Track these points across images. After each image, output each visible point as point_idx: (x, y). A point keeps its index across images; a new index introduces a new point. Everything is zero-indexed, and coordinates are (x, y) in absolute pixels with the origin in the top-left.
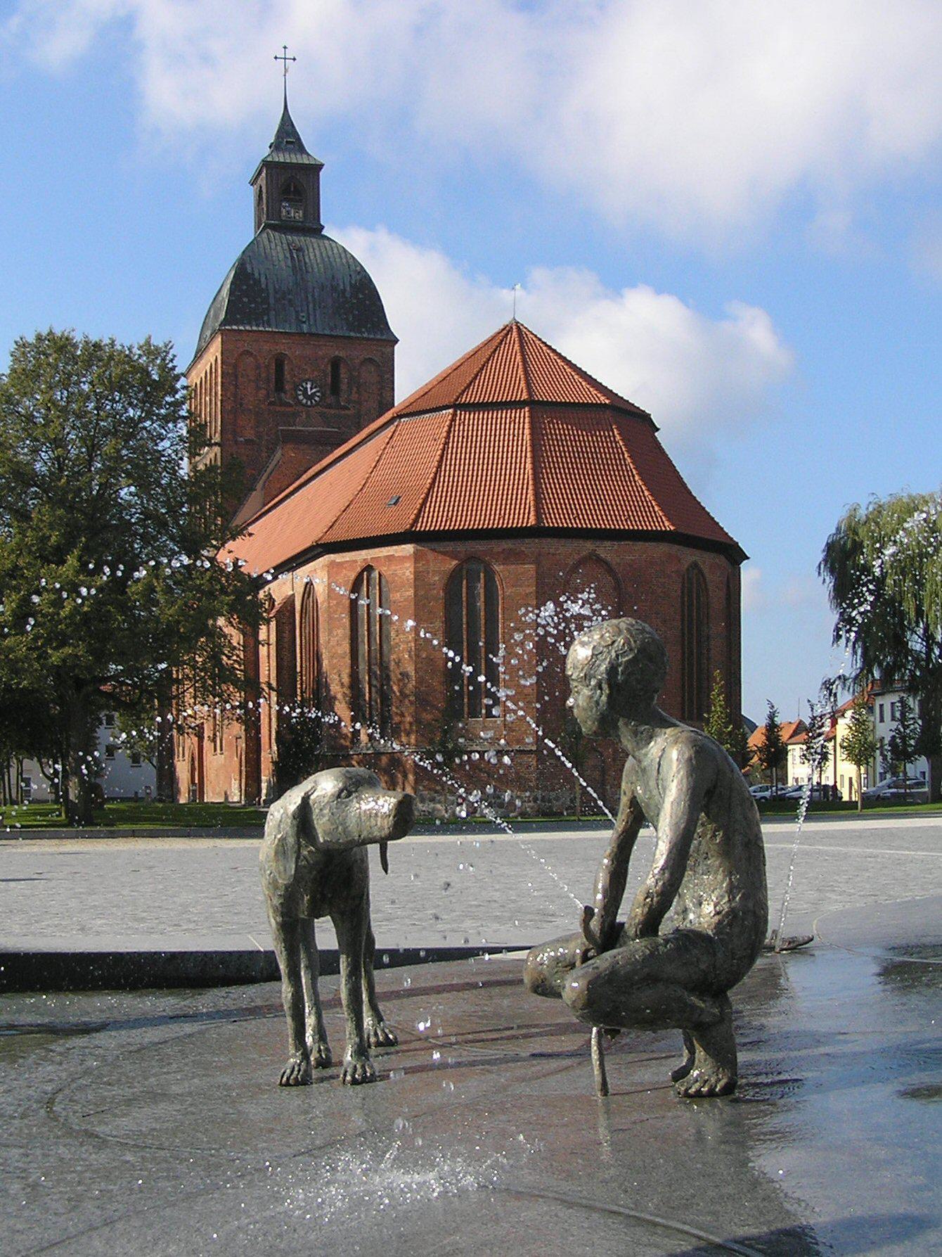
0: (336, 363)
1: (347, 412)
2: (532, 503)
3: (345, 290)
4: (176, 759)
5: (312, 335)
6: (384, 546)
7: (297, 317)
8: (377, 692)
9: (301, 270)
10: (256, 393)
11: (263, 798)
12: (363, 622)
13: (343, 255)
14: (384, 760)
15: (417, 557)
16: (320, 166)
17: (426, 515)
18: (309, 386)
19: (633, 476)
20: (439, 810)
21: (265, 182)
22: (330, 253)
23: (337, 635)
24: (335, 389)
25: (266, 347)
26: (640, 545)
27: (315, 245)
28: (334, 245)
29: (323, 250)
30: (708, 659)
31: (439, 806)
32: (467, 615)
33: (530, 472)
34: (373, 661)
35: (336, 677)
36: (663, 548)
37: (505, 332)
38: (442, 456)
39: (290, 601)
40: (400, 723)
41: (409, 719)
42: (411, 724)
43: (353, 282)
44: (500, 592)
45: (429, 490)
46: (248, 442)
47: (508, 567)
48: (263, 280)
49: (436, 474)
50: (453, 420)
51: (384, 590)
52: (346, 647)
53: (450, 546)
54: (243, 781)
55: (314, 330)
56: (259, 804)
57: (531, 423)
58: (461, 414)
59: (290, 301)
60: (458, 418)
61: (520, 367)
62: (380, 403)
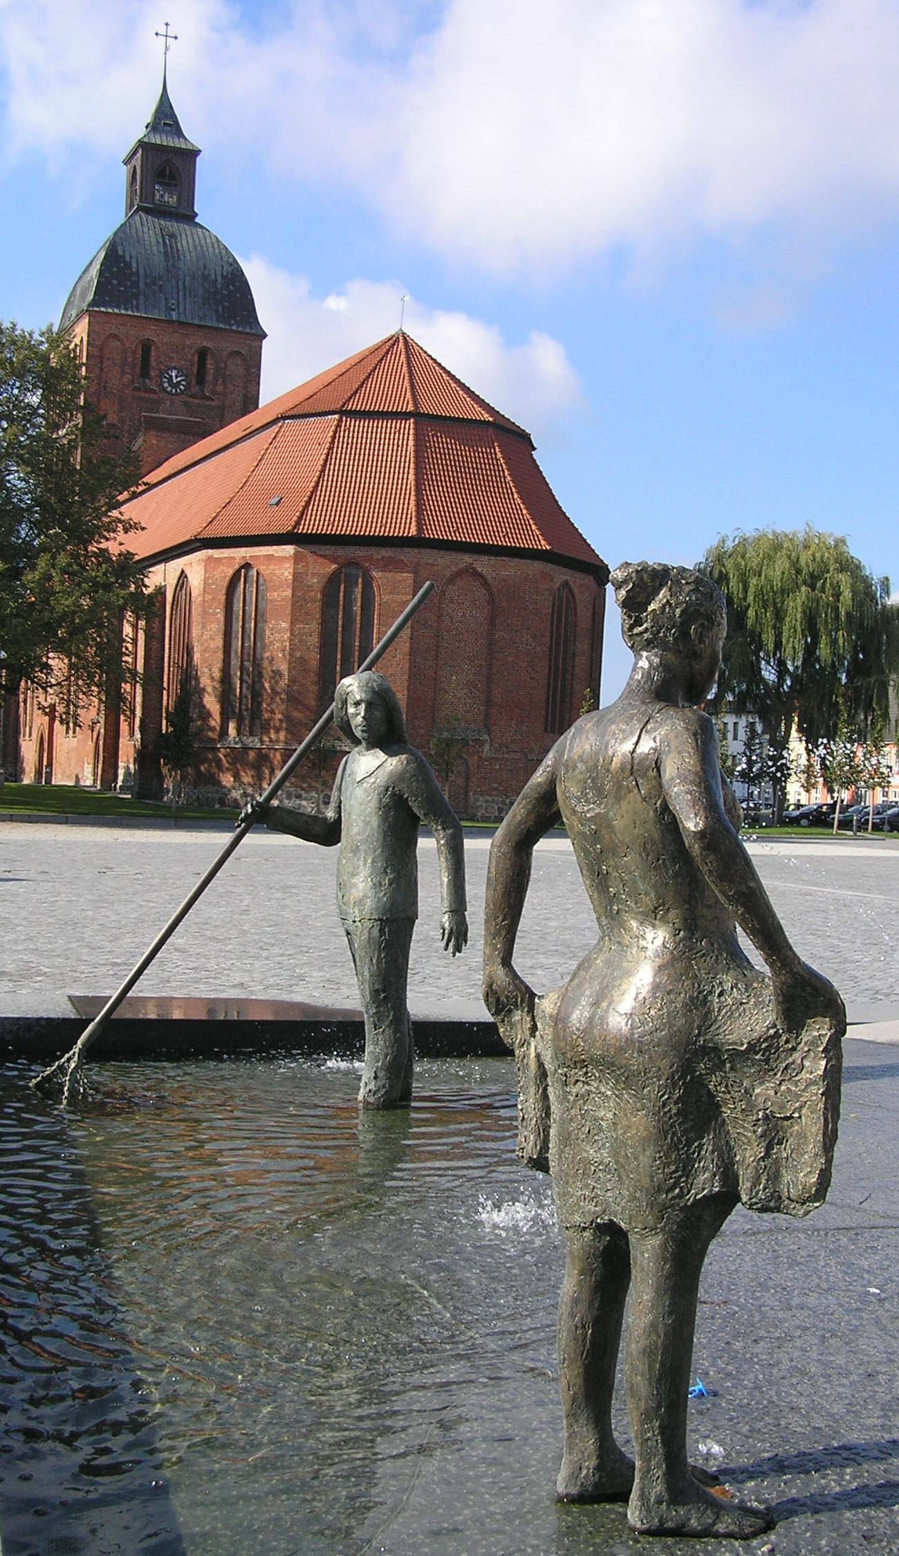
0: (203, 354)
2: (414, 514)
5: (180, 323)
7: (167, 304)
8: (248, 689)
9: (173, 257)
11: (120, 783)
12: (237, 618)
14: (252, 754)
15: (297, 558)
16: (198, 152)
18: (174, 374)
19: (512, 494)
20: (304, 807)
21: (140, 162)
22: (203, 242)
24: (201, 380)
25: (133, 332)
27: (188, 233)
29: (196, 237)
30: (572, 675)
31: (304, 803)
33: (413, 483)
34: (245, 657)
35: (207, 670)
36: (537, 566)
37: (391, 342)
38: (326, 461)
39: (161, 591)
40: (270, 720)
41: (279, 716)
42: (280, 721)
43: (225, 273)
44: (377, 599)
45: (312, 493)
47: (387, 574)
48: (134, 265)
49: (319, 478)
50: (338, 426)
51: (261, 588)
52: (219, 642)
53: (329, 550)
54: (100, 766)
55: (183, 320)
56: (115, 790)
57: (416, 435)
61: (406, 378)
62: (245, 396)
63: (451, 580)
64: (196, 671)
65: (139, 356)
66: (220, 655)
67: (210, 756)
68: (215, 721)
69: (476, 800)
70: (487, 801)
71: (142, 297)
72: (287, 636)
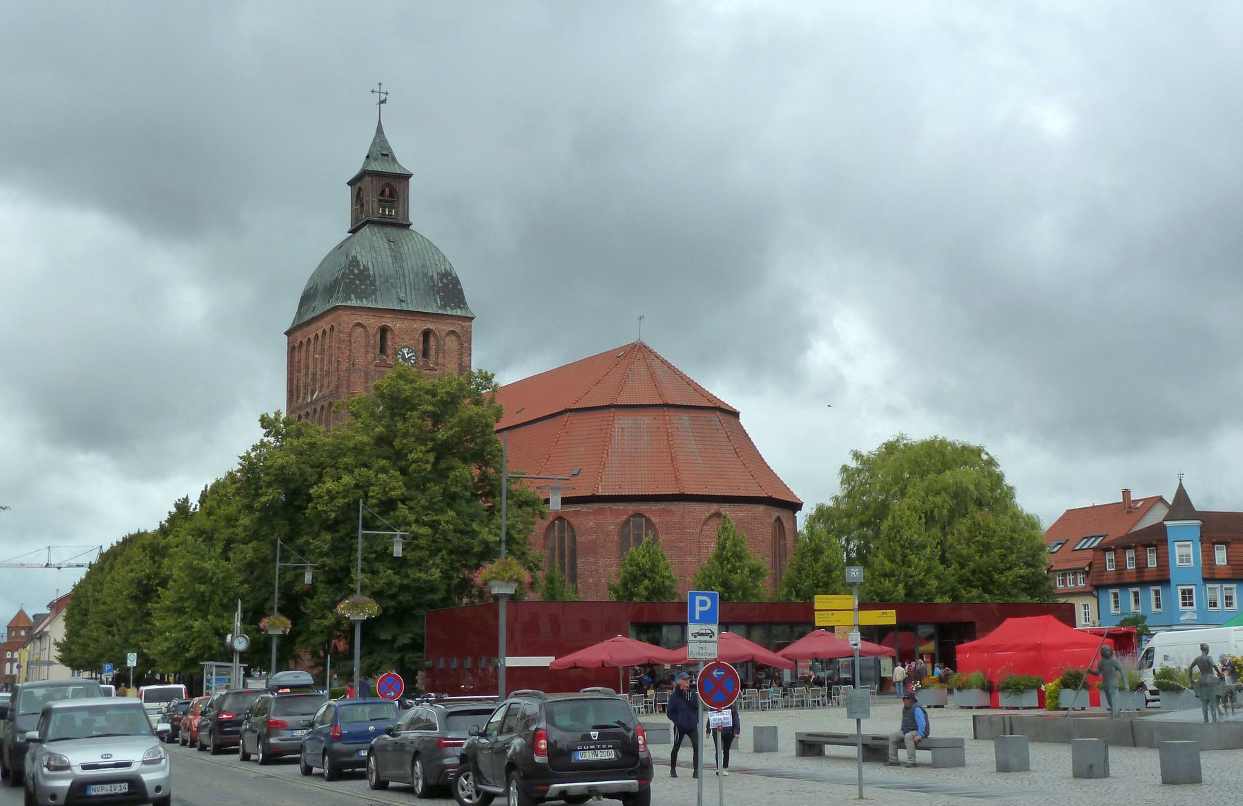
1: (435, 372)
10: (366, 356)
16: (410, 176)
18: (405, 352)
24: (425, 353)
59: (392, 283)
62: (460, 365)
63: (705, 523)
71: (378, 293)
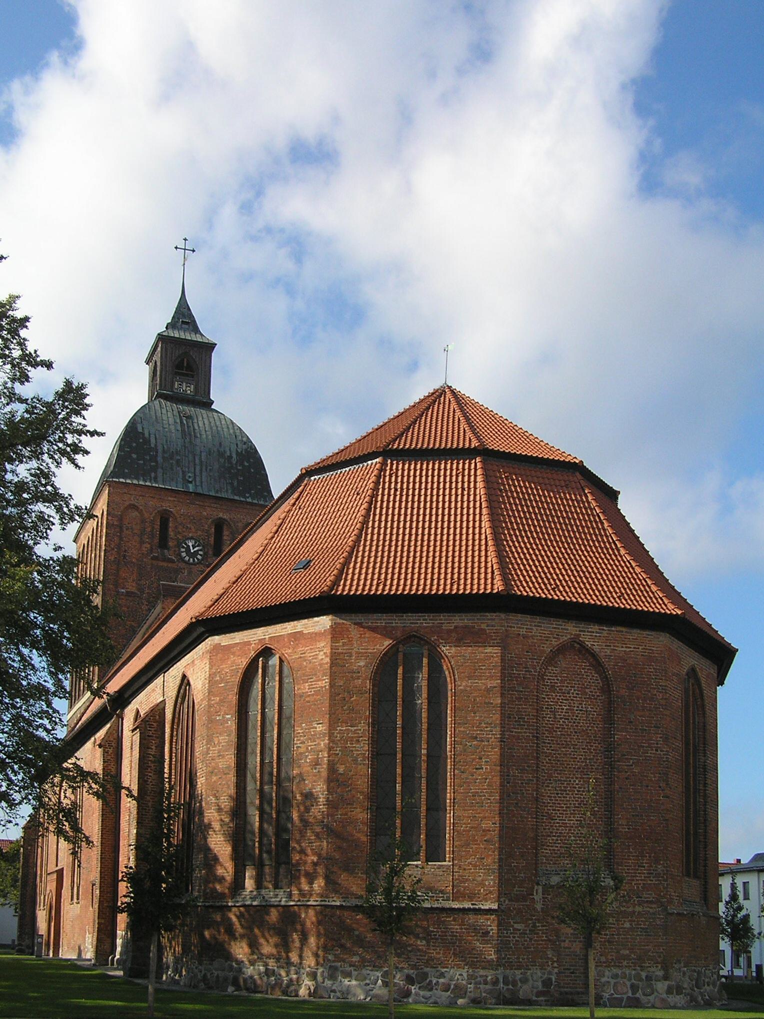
3: (231, 457)
4: (38, 908)
6: (288, 621)
9: (190, 435)
12: (255, 728)
13: (230, 427)
14: (274, 915)
15: (335, 633)
16: (211, 347)
17: (350, 577)
22: (218, 423)
23: (219, 743)
26: (636, 633)
27: (205, 416)
28: (222, 417)
29: (211, 420)
32: (403, 715)
42: (315, 864)
46: (129, 594)
48: (153, 441)
50: (382, 470)
51: (286, 680)
52: (230, 759)
53: (380, 620)
55: (199, 490)
56: (112, 964)
58: (392, 464)
60: (388, 468)
63: (552, 659)
64: (200, 802)
65: (157, 527)
66: (232, 778)
67: (218, 918)
68: (226, 869)
69: (601, 975)
70: (615, 976)
71: (160, 471)
72: (324, 743)
